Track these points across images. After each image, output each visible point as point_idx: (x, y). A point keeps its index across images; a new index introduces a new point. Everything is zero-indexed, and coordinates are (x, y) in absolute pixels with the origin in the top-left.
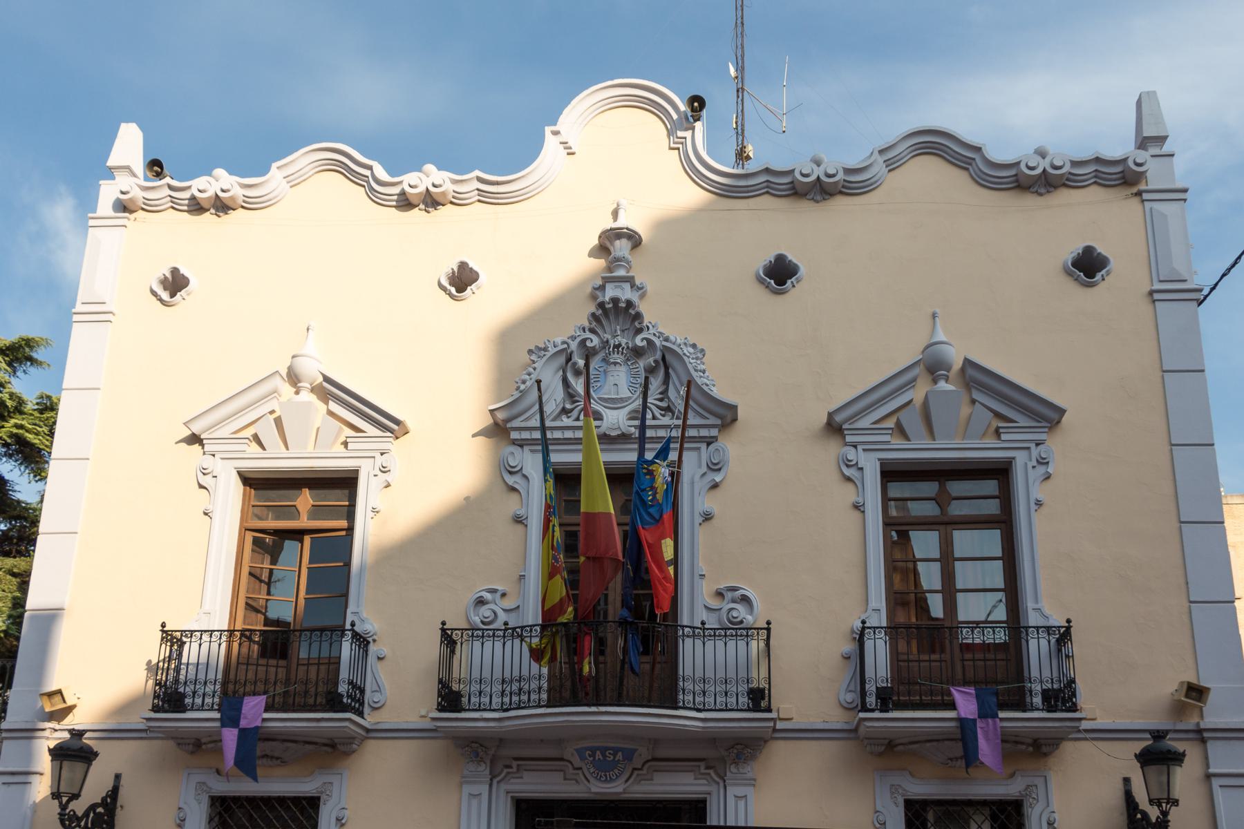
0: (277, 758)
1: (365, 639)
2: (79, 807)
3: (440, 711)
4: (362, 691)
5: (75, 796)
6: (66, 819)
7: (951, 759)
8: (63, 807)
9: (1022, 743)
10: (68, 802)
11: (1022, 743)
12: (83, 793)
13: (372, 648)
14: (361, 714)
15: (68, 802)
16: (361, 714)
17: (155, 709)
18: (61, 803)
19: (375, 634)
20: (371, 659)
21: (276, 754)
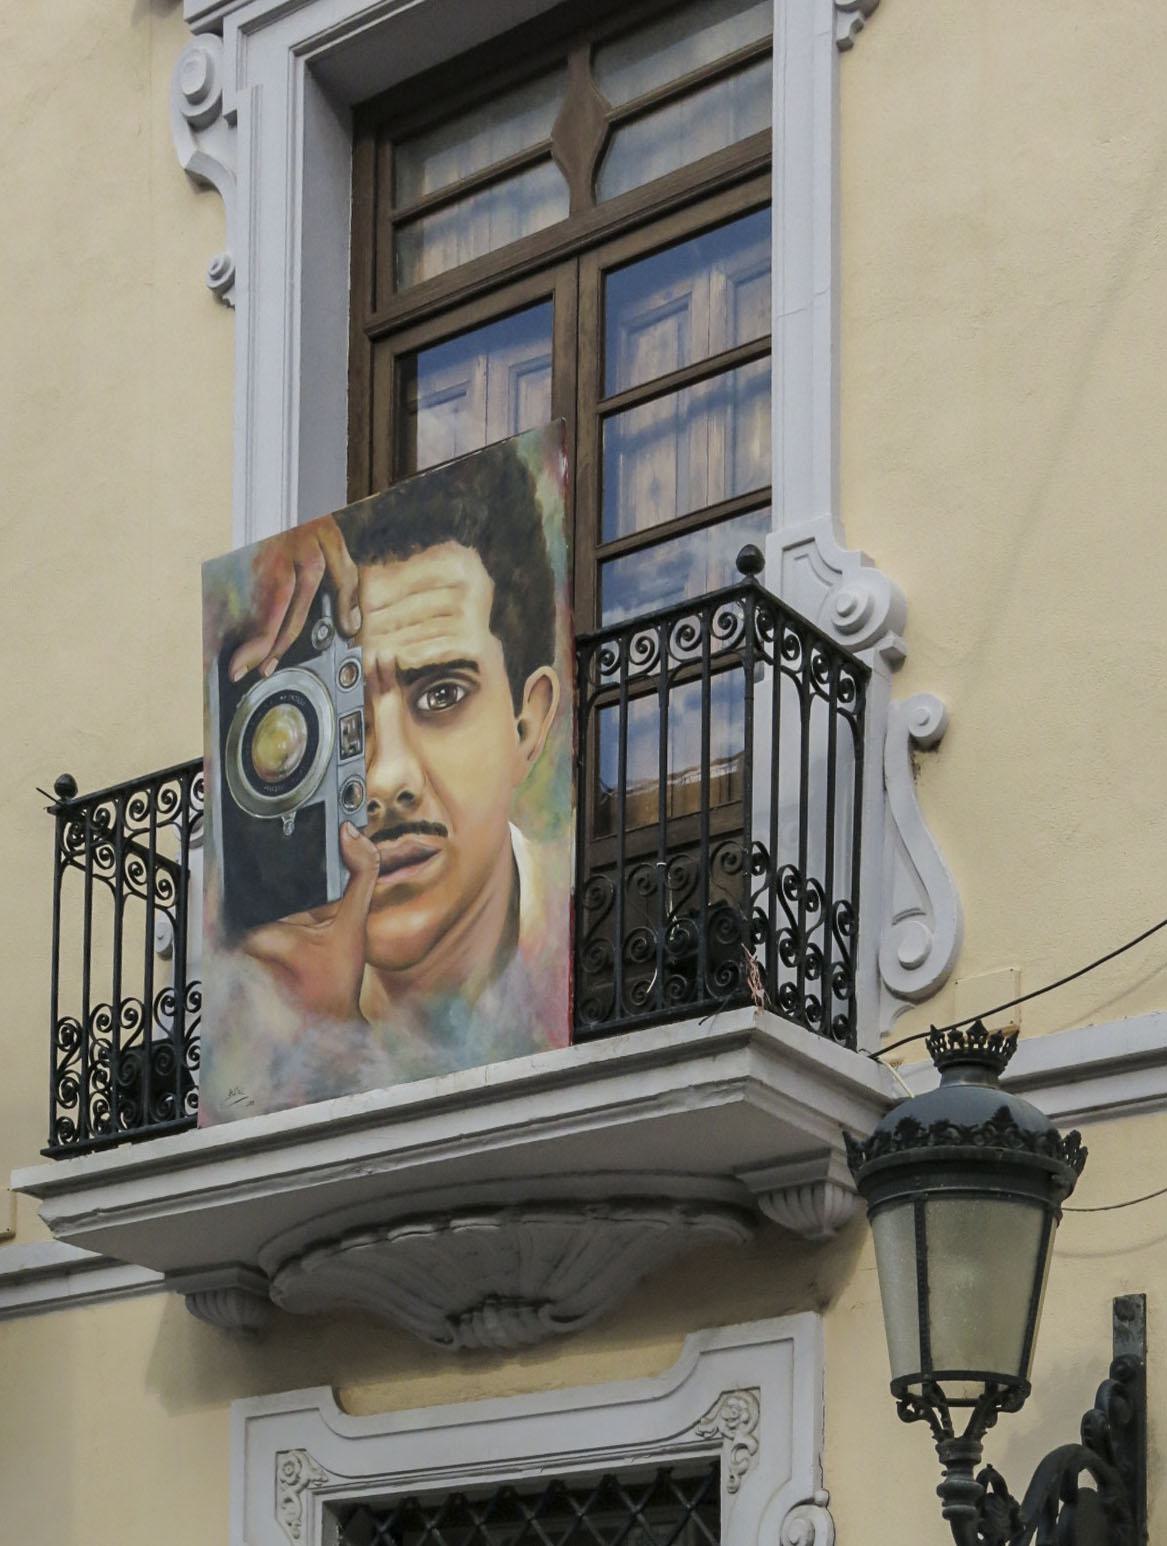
0: (536, 1304)
1: (836, 656)
2: (1015, 1450)
3: (55, 1153)
4: (844, 921)
5: (1005, 1393)
6: (973, 1503)
7: (455, 1319)
8: (959, 1454)
9: (662, 1202)
10: (976, 1430)
11: (662, 1202)
12: (1037, 1374)
13: (898, 707)
14: (843, 1031)
15: (976, 1430)
16: (843, 1031)
17: (65, 1142)
18: (942, 1434)
19: (896, 621)
20: (887, 750)
21: (528, 1287)
